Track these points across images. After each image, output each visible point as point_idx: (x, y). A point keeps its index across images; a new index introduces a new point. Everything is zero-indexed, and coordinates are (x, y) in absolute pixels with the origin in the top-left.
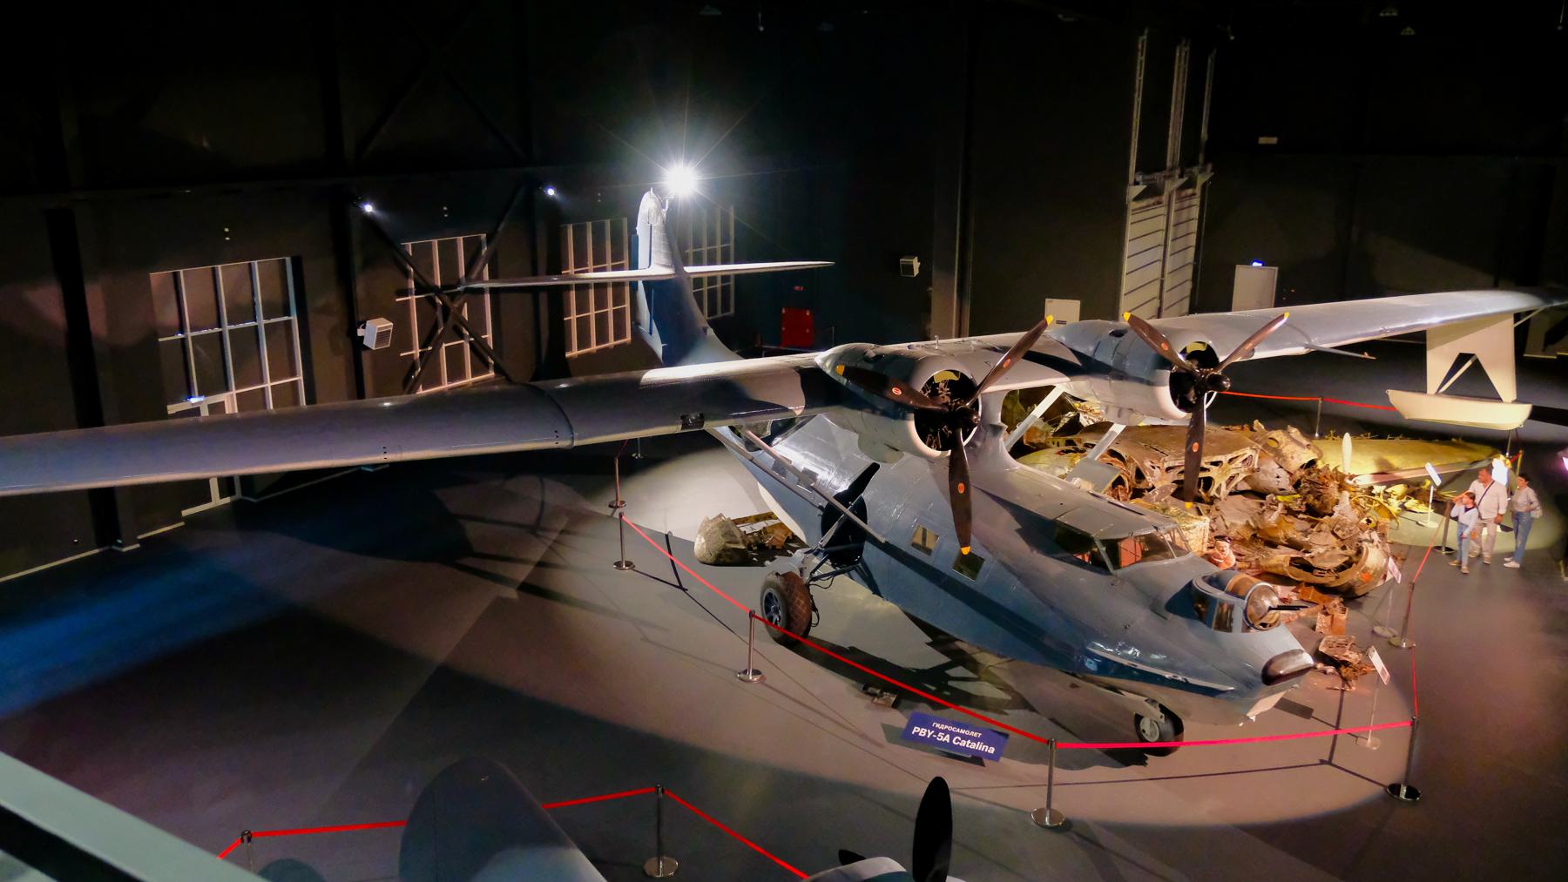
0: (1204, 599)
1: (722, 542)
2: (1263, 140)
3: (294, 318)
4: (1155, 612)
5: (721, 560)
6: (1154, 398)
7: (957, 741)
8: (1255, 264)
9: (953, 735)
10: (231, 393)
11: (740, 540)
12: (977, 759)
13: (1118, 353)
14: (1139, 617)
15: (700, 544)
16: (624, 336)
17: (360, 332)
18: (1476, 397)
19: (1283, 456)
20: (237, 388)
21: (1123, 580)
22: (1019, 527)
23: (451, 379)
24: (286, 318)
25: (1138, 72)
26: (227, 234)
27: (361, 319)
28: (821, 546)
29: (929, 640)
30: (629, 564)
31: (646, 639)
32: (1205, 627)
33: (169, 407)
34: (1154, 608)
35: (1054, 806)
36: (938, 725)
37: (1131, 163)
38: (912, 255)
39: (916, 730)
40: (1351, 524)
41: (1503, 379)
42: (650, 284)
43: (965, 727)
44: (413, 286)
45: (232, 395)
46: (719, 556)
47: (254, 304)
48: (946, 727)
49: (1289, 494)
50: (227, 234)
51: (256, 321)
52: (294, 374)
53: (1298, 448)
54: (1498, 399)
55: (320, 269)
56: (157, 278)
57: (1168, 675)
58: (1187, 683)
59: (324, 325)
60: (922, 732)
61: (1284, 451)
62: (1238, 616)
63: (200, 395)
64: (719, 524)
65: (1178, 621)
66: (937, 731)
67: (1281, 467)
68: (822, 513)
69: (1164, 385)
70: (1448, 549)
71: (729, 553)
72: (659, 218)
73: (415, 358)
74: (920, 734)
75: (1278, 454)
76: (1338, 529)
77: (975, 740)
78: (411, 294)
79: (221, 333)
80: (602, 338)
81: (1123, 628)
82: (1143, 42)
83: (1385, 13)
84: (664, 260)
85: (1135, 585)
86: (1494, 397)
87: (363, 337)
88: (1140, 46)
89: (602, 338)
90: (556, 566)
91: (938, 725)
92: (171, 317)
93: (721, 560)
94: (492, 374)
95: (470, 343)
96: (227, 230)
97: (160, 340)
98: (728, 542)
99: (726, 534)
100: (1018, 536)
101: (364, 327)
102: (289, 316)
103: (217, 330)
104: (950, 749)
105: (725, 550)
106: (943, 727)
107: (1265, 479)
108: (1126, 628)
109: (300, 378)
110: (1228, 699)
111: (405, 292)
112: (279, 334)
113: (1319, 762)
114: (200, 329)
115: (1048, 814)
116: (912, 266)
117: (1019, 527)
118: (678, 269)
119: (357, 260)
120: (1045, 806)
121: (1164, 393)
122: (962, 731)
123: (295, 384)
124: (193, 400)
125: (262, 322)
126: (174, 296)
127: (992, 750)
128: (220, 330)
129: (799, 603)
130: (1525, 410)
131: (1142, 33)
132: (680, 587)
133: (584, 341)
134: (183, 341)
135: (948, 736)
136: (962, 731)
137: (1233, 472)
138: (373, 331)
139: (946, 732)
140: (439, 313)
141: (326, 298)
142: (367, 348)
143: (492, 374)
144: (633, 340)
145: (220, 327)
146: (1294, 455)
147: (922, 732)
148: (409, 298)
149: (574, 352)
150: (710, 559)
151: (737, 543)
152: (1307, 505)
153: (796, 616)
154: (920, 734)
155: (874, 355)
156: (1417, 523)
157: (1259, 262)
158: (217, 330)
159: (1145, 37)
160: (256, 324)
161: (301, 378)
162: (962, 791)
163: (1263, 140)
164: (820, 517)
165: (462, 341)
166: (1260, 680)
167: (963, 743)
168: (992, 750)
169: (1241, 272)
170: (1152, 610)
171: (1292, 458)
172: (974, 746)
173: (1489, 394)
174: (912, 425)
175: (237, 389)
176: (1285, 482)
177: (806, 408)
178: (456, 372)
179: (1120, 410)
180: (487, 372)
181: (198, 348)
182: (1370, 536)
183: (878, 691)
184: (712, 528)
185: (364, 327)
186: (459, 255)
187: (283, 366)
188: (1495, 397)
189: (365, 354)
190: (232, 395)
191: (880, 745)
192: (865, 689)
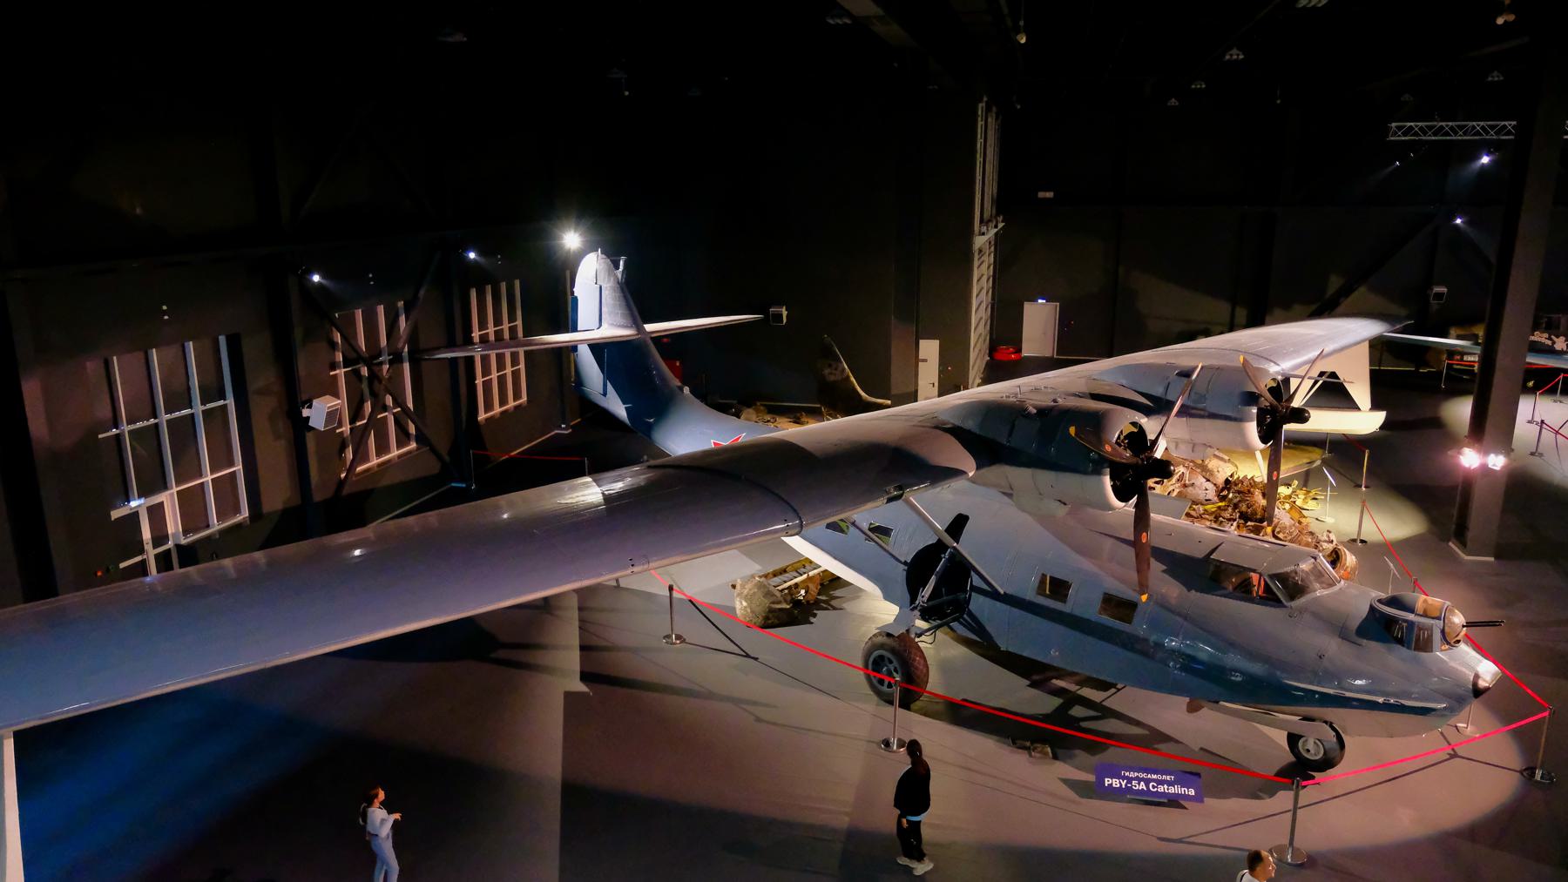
0: (1390, 622)
1: (766, 602)
2: (1041, 195)
3: (230, 402)
4: (1345, 639)
5: (770, 622)
6: (1242, 435)
7: (1154, 787)
8: (1040, 301)
9: (1147, 782)
10: (172, 491)
11: (782, 599)
12: (1174, 802)
13: (1196, 393)
14: (1332, 646)
15: (740, 606)
16: (520, 398)
17: (306, 412)
18: (1339, 408)
19: (1209, 470)
20: (178, 483)
21: (1302, 610)
22: (1165, 567)
23: (379, 455)
24: (221, 403)
25: (979, 136)
26: (165, 313)
27: (304, 397)
28: (923, 602)
29: (1028, 682)
30: (678, 637)
31: (758, 720)
32: (1404, 649)
33: (112, 513)
34: (1343, 633)
35: (1296, 844)
36: (1127, 774)
37: (976, 216)
38: (781, 305)
39: (1107, 781)
40: (1290, 527)
41: (1361, 392)
42: (597, 348)
43: (1155, 772)
44: (341, 359)
45: (173, 493)
46: (767, 618)
47: (189, 389)
48: (1136, 774)
49: (1213, 504)
50: (165, 313)
51: (191, 408)
52: (232, 464)
53: (1221, 463)
54: (1359, 409)
55: (257, 347)
56: (93, 367)
57: (1381, 700)
58: (1403, 706)
59: (263, 408)
60: (1116, 783)
61: (1210, 466)
62: (1437, 636)
63: (140, 497)
64: (755, 585)
65: (1374, 646)
66: (1130, 780)
67: (1208, 480)
68: (906, 568)
69: (1252, 421)
70: (1362, 541)
71: (776, 614)
72: (612, 279)
73: (345, 435)
74: (1114, 785)
75: (1204, 469)
76: (1279, 533)
77: (1170, 784)
78: (339, 368)
79: (156, 425)
80: (503, 401)
81: (1318, 658)
82: (982, 108)
83: (1493, 77)
84: (620, 320)
85: (1316, 615)
86: (1352, 405)
87: (308, 418)
88: (980, 113)
89: (503, 401)
90: (555, 647)
91: (1127, 774)
92: (104, 412)
93: (770, 622)
94: (413, 445)
95: (394, 414)
96: (165, 308)
97: (100, 436)
98: (773, 603)
99: (766, 594)
100: (1167, 576)
101: (310, 407)
102: (225, 400)
103: (152, 421)
104: (1148, 796)
105: (771, 611)
106: (1132, 775)
107: (1194, 492)
108: (1320, 657)
109: (238, 467)
110: (1438, 716)
111: (334, 366)
112: (216, 419)
113: (1448, 757)
114: (135, 423)
115: (1290, 851)
116: (782, 315)
117: (1165, 567)
118: (640, 330)
119: (298, 333)
120: (1286, 841)
121: (1252, 429)
122: (1154, 777)
123: (233, 475)
124: (134, 504)
125: (198, 408)
126: (106, 388)
127: (1192, 792)
128: (156, 421)
129: (919, 663)
130: (1380, 417)
131: (981, 101)
132: (747, 656)
133: (489, 407)
134: (118, 438)
135: (1142, 783)
136: (1154, 777)
137: (1171, 488)
138: (318, 413)
139: (1139, 780)
140: (365, 386)
141: (263, 377)
142: (312, 429)
143: (413, 445)
144: (528, 401)
145: (155, 418)
146: (1220, 469)
147: (1116, 783)
148: (337, 372)
149: (482, 416)
150: (760, 621)
151: (779, 602)
152: (1241, 513)
153: (918, 677)
154: (1114, 785)
155: (1035, 411)
156: (1317, 519)
157: (1043, 299)
158: (152, 421)
159: (984, 104)
160: (193, 411)
161: (241, 467)
162: (1191, 840)
163: (1041, 195)
164: (905, 573)
165: (386, 414)
166: (1472, 695)
167: (1161, 789)
168: (1192, 792)
169: (1028, 308)
170: (1343, 638)
171: (1218, 471)
172: (1172, 790)
173: (1349, 404)
174: (1107, 481)
175: (177, 486)
176: (1211, 493)
177: (977, 469)
178: (382, 448)
179: (1194, 445)
180: (408, 444)
181: (134, 443)
182: (1329, 537)
183: (1028, 744)
184: (750, 590)
185: (310, 407)
186: (380, 320)
187: (221, 458)
188: (1352, 405)
189: (309, 436)
190: (173, 493)
191: (1074, 802)
192: (1014, 743)
